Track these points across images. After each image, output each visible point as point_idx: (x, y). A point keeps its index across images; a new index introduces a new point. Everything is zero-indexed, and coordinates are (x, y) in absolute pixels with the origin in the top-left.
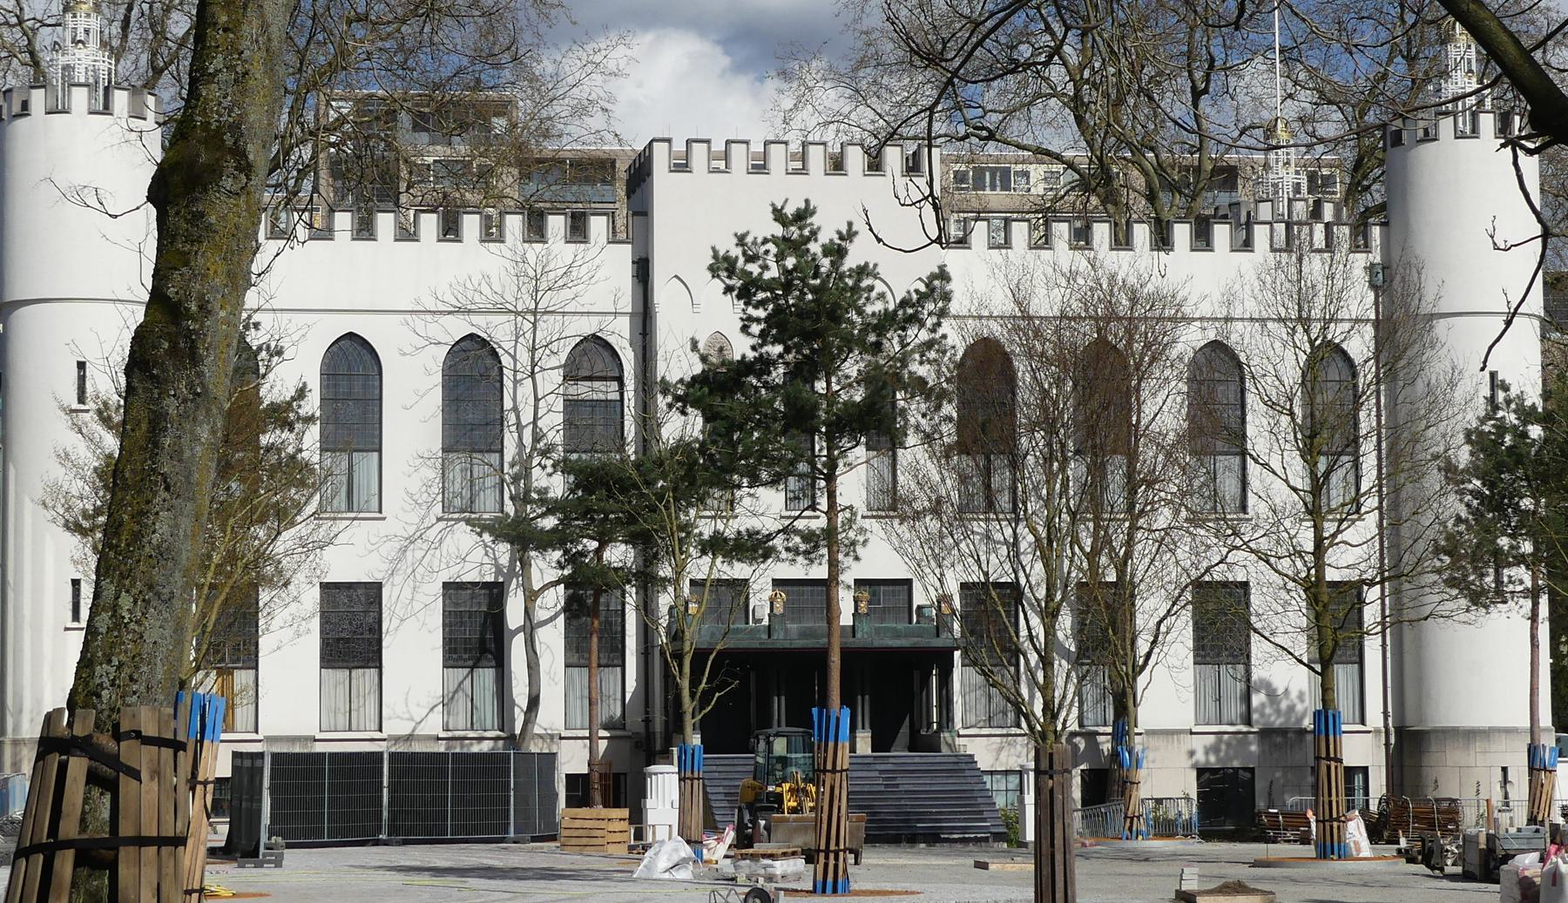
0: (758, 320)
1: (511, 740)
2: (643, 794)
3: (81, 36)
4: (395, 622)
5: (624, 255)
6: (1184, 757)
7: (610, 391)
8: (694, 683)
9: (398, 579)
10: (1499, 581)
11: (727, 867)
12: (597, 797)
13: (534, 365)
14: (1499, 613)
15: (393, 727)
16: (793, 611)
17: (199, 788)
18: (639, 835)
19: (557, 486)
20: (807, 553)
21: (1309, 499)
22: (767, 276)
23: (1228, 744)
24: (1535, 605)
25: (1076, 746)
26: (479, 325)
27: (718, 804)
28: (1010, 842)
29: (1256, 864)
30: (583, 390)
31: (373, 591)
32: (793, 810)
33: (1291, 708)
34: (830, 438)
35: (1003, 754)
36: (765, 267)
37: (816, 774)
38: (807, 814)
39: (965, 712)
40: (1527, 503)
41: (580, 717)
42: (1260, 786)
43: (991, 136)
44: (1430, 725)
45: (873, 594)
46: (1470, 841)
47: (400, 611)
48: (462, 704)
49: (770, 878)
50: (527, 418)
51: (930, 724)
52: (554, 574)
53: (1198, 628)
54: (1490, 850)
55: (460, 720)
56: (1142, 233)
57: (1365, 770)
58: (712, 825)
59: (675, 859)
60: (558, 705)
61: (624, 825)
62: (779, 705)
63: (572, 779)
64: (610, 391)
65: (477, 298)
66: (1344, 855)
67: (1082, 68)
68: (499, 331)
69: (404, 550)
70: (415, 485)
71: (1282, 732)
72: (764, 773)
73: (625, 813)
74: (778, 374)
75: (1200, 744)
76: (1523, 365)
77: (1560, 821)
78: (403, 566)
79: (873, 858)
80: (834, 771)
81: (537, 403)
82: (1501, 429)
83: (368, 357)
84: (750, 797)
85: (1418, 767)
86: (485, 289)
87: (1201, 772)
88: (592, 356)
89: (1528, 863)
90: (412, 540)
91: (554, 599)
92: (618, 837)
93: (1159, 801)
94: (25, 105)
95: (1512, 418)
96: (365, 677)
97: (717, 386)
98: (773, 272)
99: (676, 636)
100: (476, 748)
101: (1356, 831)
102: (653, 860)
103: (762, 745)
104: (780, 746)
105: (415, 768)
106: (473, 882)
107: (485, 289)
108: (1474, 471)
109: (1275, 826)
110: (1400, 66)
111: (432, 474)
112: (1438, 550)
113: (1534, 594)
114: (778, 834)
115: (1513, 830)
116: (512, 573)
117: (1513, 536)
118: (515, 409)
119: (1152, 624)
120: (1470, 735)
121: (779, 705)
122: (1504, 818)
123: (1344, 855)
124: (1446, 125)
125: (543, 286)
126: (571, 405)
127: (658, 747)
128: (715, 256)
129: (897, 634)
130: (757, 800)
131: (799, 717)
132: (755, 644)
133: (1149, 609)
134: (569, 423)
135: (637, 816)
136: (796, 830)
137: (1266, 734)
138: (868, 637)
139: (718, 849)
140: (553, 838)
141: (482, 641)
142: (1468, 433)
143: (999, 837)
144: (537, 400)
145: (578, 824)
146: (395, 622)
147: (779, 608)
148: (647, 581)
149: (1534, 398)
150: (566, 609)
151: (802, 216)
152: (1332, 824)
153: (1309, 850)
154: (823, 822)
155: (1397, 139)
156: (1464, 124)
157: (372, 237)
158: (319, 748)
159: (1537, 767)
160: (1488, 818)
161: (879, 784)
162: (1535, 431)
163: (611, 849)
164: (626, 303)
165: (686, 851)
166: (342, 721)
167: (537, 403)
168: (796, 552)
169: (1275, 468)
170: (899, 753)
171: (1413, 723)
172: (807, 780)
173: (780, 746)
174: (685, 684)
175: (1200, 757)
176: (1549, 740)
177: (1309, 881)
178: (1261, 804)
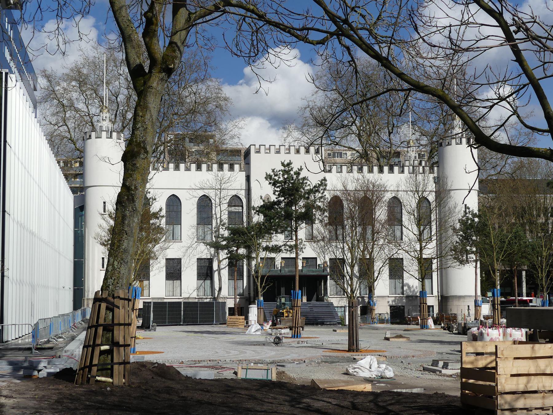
0: (277, 191)
1: (215, 299)
2: (248, 312)
3: (104, 118)
4: (185, 268)
5: (243, 174)
7: (239, 209)
8: (261, 284)
9: (185, 257)
10: (467, 258)
11: (270, 331)
12: (236, 313)
13: (220, 203)
15: (184, 295)
16: (286, 265)
17: (135, 311)
18: (247, 323)
19: (226, 234)
20: (290, 251)
21: (418, 237)
22: (280, 180)
23: (398, 300)
25: (359, 300)
26: (206, 192)
27: (267, 315)
28: (342, 325)
29: (405, 330)
30: (233, 209)
31: (178, 261)
33: (414, 290)
35: (340, 302)
36: (279, 178)
37: (292, 307)
39: (330, 291)
40: (474, 238)
41: (232, 292)
42: (406, 310)
43: (337, 144)
45: (307, 261)
46: (460, 324)
47: (186, 265)
48: (202, 289)
49: (281, 334)
50: (218, 216)
51: (321, 295)
52: (225, 256)
53: (391, 270)
54: (465, 327)
55: (201, 293)
57: (433, 306)
58: (266, 321)
59: (256, 329)
60: (227, 290)
61: (243, 320)
62: (283, 290)
63: (230, 309)
64: (239, 209)
66: (427, 328)
67: (360, 126)
68: (211, 194)
69: (187, 250)
70: (190, 233)
71: (412, 296)
73: (243, 317)
74: (283, 205)
75: (390, 300)
77: (483, 319)
78: (187, 254)
79: (307, 329)
80: (297, 306)
81: (221, 212)
82: (468, 219)
83: (178, 201)
84: (275, 313)
85: (446, 305)
87: (391, 307)
88: (235, 200)
91: (225, 262)
93: (380, 314)
94: (90, 136)
95: (470, 216)
97: (267, 208)
98: (281, 179)
99: (257, 272)
100: (205, 301)
101: (430, 322)
102: (251, 329)
103: (279, 300)
104: (283, 300)
106: (205, 335)
108: (461, 230)
109: (410, 321)
110: (442, 126)
111: (194, 230)
113: (476, 261)
114: (283, 323)
115: (471, 322)
117: (471, 246)
118: (215, 214)
119: (378, 269)
120: (460, 297)
121: (283, 290)
122: (468, 319)
123: (427, 328)
124: (453, 141)
125: (223, 182)
126: (230, 213)
128: (267, 175)
129: (313, 271)
130: (277, 314)
131: (288, 293)
132: (277, 274)
133: (377, 265)
134: (229, 218)
135: (247, 318)
136: (287, 322)
137: (408, 297)
139: (267, 326)
140: (225, 324)
141: (207, 273)
142: (459, 220)
143: (339, 323)
144: (221, 211)
145: (231, 320)
146: (185, 268)
147: (283, 265)
148: (249, 258)
149: (476, 211)
150: (228, 265)
151: (289, 164)
152: (424, 320)
158: (165, 301)
159: (477, 305)
161: (308, 310)
162: (476, 220)
164: (244, 187)
165: (259, 327)
166: (171, 294)
167: (221, 212)
169: (410, 229)
170: (314, 302)
171: (445, 294)
173: (283, 300)
174: (259, 284)
175: (391, 303)
176: (480, 299)
177: (419, 335)
178: (406, 315)
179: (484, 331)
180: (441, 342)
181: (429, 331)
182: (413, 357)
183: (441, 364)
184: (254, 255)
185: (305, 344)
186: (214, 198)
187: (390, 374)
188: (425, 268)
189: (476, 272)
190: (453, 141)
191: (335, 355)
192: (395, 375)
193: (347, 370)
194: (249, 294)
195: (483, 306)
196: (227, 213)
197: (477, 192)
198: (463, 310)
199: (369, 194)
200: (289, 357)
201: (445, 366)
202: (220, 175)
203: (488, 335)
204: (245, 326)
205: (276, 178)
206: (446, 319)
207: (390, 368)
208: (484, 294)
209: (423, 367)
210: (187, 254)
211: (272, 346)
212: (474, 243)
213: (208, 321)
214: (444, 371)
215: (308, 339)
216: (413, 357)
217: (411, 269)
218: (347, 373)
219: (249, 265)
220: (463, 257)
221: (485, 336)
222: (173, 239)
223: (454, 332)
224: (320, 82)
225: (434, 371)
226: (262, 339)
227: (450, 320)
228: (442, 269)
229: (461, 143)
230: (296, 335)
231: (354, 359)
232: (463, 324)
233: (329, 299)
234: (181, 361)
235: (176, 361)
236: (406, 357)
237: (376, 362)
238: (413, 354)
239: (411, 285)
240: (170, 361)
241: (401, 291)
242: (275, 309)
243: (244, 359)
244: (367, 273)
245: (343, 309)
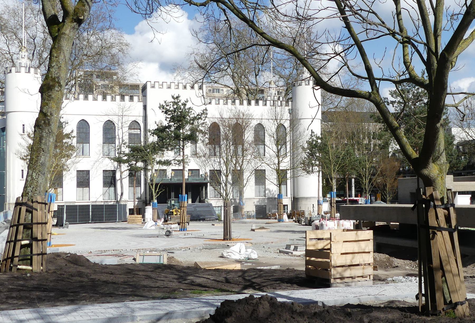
2: (145, 212)
4: (93, 178)
5: (141, 104)
7: (138, 132)
8: (155, 190)
9: (93, 169)
10: (312, 169)
11: (162, 226)
12: (135, 213)
14: (312, 175)
15: (92, 199)
19: (127, 151)
29: (267, 223)
30: (133, 131)
32: (176, 215)
33: (273, 194)
34: (183, 141)
36: (170, 107)
37: (180, 208)
38: (178, 215)
40: (318, 155)
46: (306, 218)
48: (107, 195)
50: (121, 137)
54: (310, 220)
58: (159, 218)
61: (141, 218)
62: (173, 194)
63: (130, 210)
64: (138, 132)
65: (110, 113)
68: (115, 119)
69: (94, 163)
71: (272, 198)
72: (170, 208)
73: (141, 216)
74: (173, 129)
75: (256, 201)
77: (323, 214)
79: (192, 224)
81: (123, 134)
82: (313, 140)
84: (167, 212)
87: (256, 206)
88: (134, 125)
91: (127, 173)
92: (139, 221)
93: (248, 212)
94: (11, 71)
95: (315, 139)
96: (86, 189)
97: (160, 131)
98: (172, 109)
99: (152, 181)
100: (110, 204)
101: (285, 217)
103: (169, 202)
105: (97, 208)
106: (109, 230)
108: (308, 148)
111: (101, 148)
113: (319, 171)
120: (307, 198)
121: (173, 194)
122: (313, 214)
125: (124, 110)
126: (130, 134)
127: (148, 202)
129: (197, 180)
130: (168, 213)
131: (177, 196)
132: (168, 182)
133: (246, 175)
137: (269, 198)
138: (191, 181)
139: (160, 222)
140: (126, 221)
141: (111, 182)
143: (217, 219)
147: (173, 175)
148: (146, 169)
149: (319, 135)
150: (129, 175)
151: (177, 98)
154: (182, 217)
155: (294, 86)
159: (319, 204)
161: (193, 209)
162: (319, 141)
163: (138, 223)
165: (154, 223)
166: (81, 198)
167: (123, 134)
169: (270, 147)
170: (197, 203)
173: (173, 202)
174: (154, 190)
175: (256, 203)
176: (321, 199)
178: (267, 212)
179: (323, 223)
182: (272, 243)
183: (292, 247)
184: (149, 167)
185: (190, 236)
186: (117, 122)
189: (319, 180)
192: (259, 257)
193: (222, 254)
194: (146, 198)
196: (128, 134)
197: (320, 121)
198: (309, 208)
201: (296, 249)
202: (122, 105)
203: (327, 225)
204: (142, 223)
205: (168, 108)
206: (296, 214)
208: (324, 196)
212: (318, 159)
214: (295, 253)
215: (192, 232)
216: (272, 243)
217: (272, 177)
218: (222, 257)
219: (146, 175)
222: (83, 155)
225: (287, 253)
226: (156, 232)
230: (183, 229)
231: (228, 246)
234: (89, 251)
238: (272, 241)
240: (81, 251)
242: (166, 209)
243: (142, 248)
245: (220, 208)
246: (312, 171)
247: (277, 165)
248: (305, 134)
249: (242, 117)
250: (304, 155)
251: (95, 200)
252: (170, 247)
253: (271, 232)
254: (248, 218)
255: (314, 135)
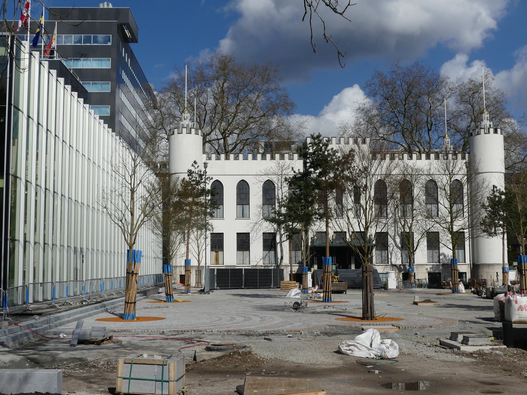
3: (185, 118)
6: (425, 270)
9: (253, 232)
10: (495, 231)
14: (495, 238)
15: (252, 263)
19: (284, 210)
20: (320, 219)
21: (449, 209)
24: (504, 236)
29: (438, 294)
31: (248, 234)
40: (501, 213)
42: (442, 276)
44: (480, 263)
46: (487, 289)
47: (254, 239)
48: (267, 258)
53: (428, 242)
54: (493, 291)
55: (267, 262)
56: (414, 156)
57: (466, 273)
59: (296, 293)
65: (270, 172)
68: (274, 179)
75: (429, 267)
76: (501, 186)
77: (510, 284)
80: (327, 272)
82: (495, 196)
85: (477, 272)
86: (271, 170)
87: (429, 274)
89: (501, 296)
90: (256, 223)
94: (173, 132)
95: (498, 194)
100: (270, 268)
101: (461, 287)
107: (271, 170)
108: (489, 206)
109: (445, 285)
112: (481, 224)
113: (503, 233)
115: (498, 287)
116: (277, 231)
119: (417, 241)
120: (489, 265)
122: (496, 284)
133: (416, 237)
137: (443, 265)
140: (280, 288)
141: (271, 245)
142: (488, 198)
143: (382, 288)
147: (334, 238)
149: (503, 190)
151: (319, 136)
152: (455, 285)
153: (450, 291)
155: (471, 134)
156: (486, 131)
157: (247, 159)
158: (237, 268)
159: (504, 272)
160: (493, 284)
162: (503, 197)
166: (242, 262)
168: (317, 218)
172: (335, 275)
175: (429, 270)
176: (507, 266)
177: (449, 299)
178: (442, 280)
179: (511, 298)
180: (469, 307)
181: (460, 295)
182: (431, 327)
183: (460, 338)
187: (393, 353)
188: (458, 240)
189: (503, 243)
190: (482, 130)
191: (347, 325)
192: (401, 354)
193: (339, 348)
195: (510, 272)
197: (503, 175)
198: (493, 277)
199: (408, 178)
200: (283, 328)
201: (465, 341)
202: (281, 163)
203: (516, 302)
206: (476, 283)
207: (396, 344)
208: (510, 264)
209: (440, 341)
210: (255, 229)
211: (291, 311)
213: (266, 285)
214: (463, 348)
216: (431, 327)
217: (446, 239)
218: (339, 352)
220: (491, 229)
221: (513, 303)
223: (483, 296)
224: (369, 89)
225: (451, 347)
227: (480, 285)
228: (473, 238)
229: (489, 132)
232: (491, 289)
233: (374, 266)
234: (162, 331)
235: (156, 331)
236: (423, 327)
237: (379, 337)
238: (431, 324)
239: (446, 254)
241: (437, 259)
244: (407, 244)
246: (495, 233)
247: (450, 224)
248: (485, 186)
249: (410, 173)
250: (484, 214)
251: (255, 264)
252: (276, 329)
253: (439, 306)
254: (418, 287)
255: (497, 190)
